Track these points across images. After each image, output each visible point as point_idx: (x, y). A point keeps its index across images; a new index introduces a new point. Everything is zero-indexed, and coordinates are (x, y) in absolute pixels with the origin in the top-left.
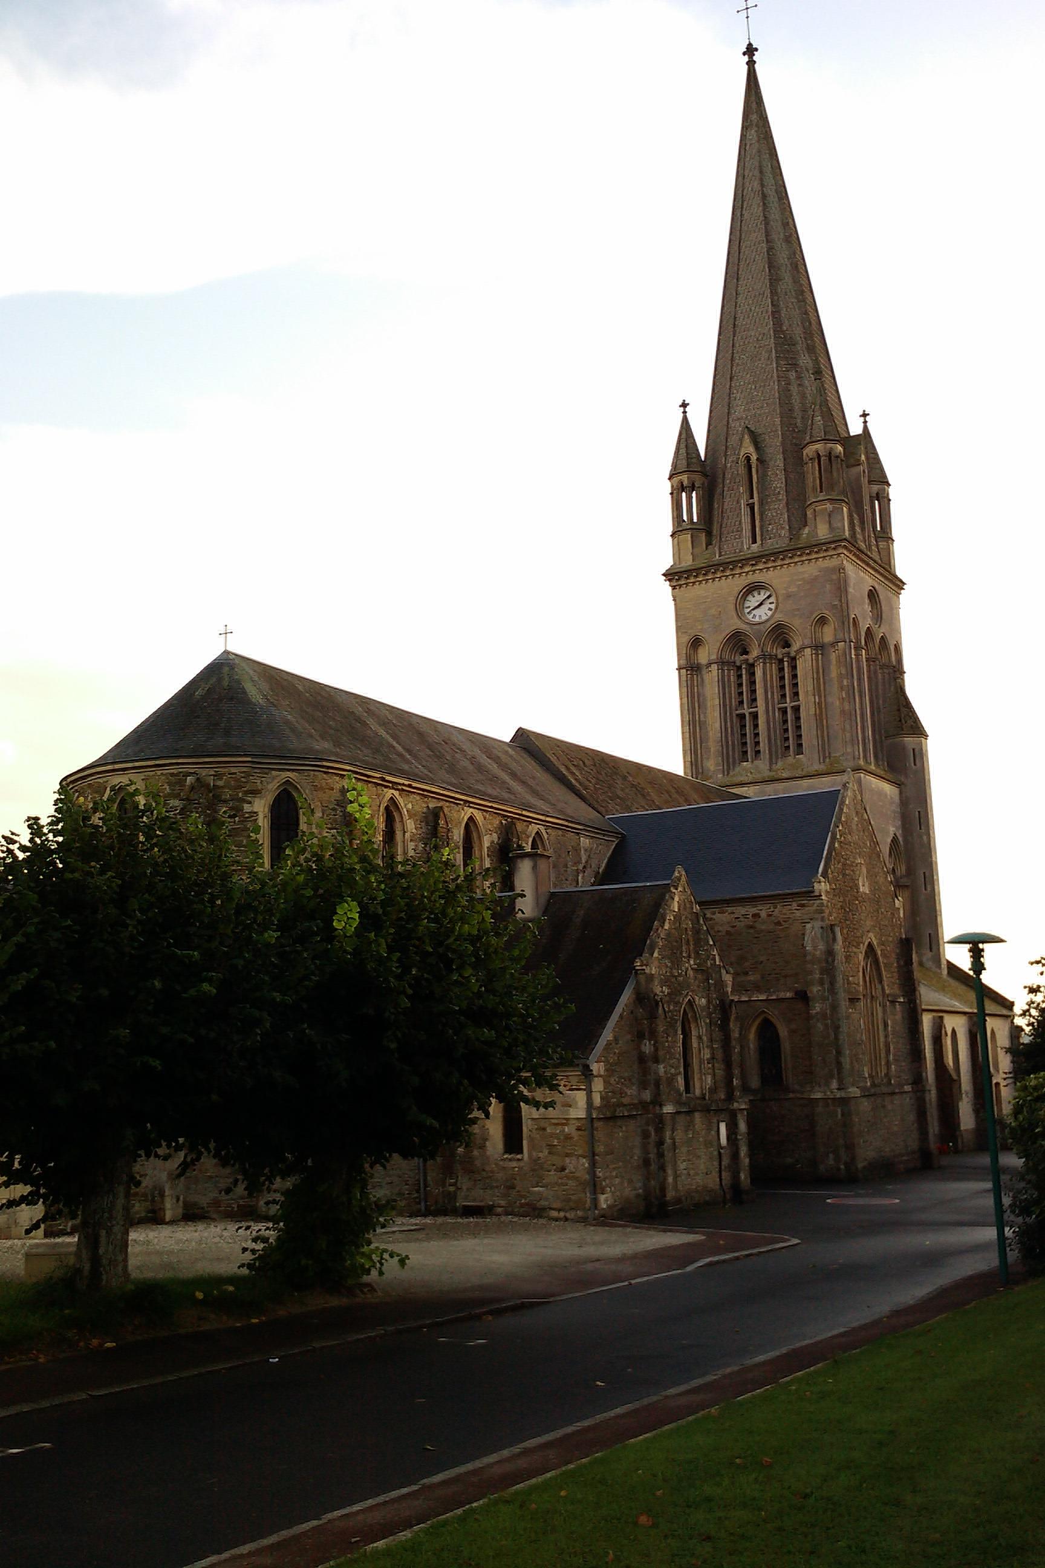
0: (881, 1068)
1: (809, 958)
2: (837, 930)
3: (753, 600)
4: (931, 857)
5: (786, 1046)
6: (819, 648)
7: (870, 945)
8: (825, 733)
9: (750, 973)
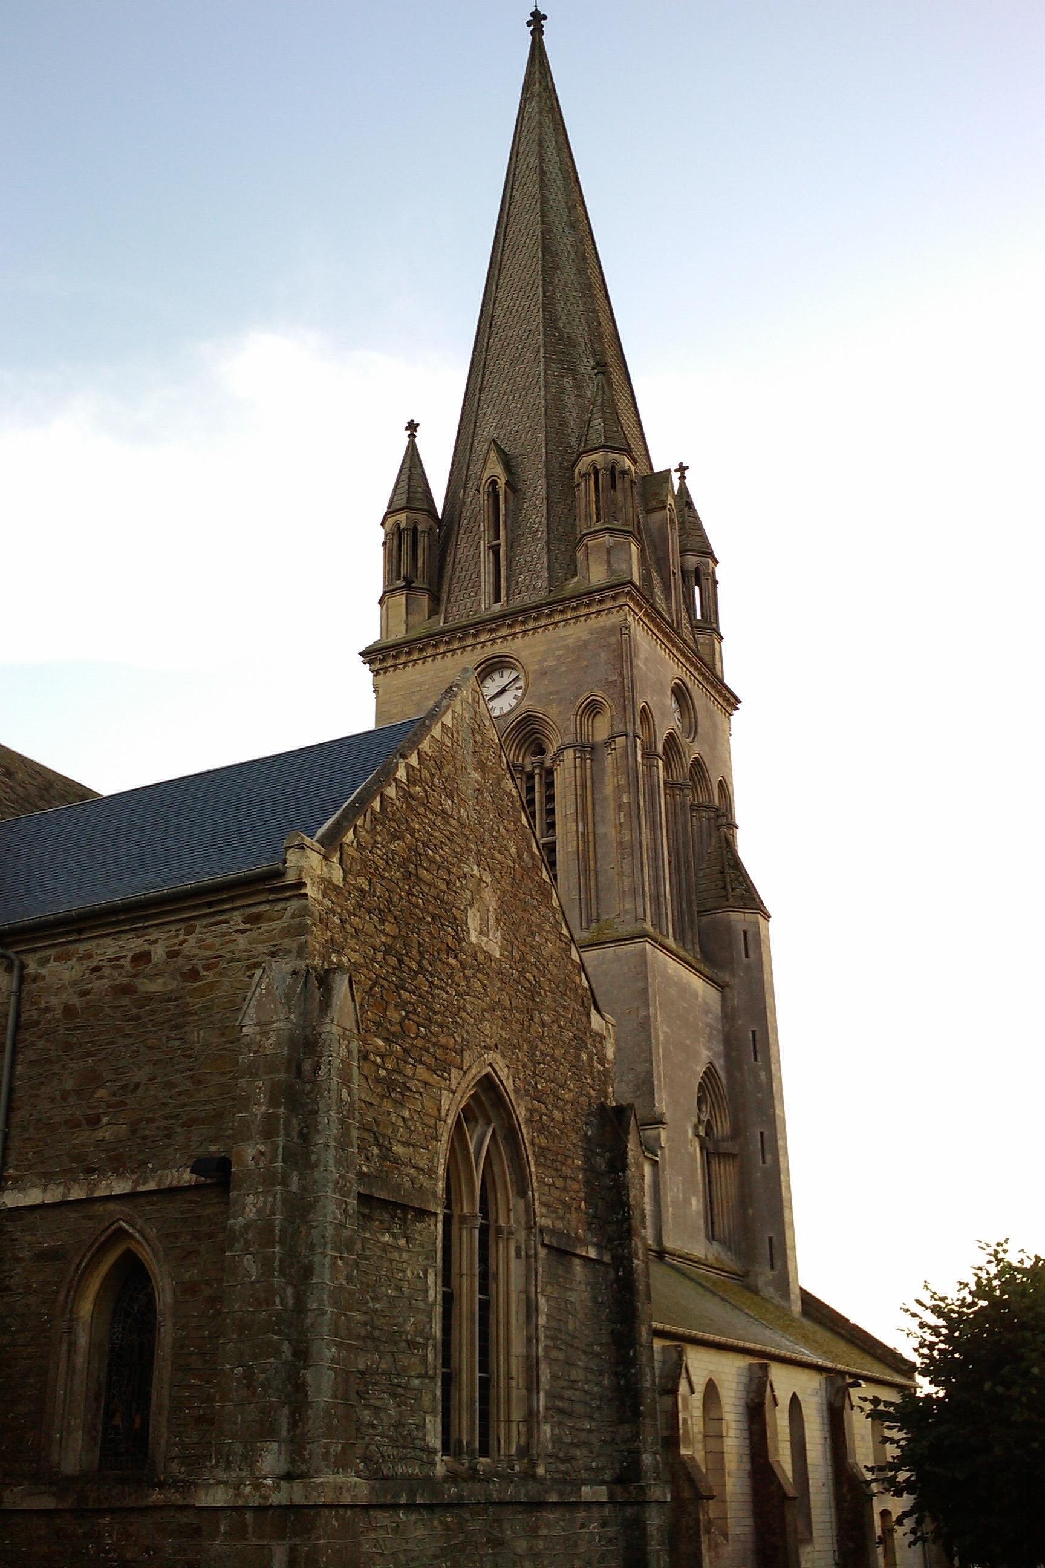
0: (509, 1431)
1: (246, 1058)
2: (341, 986)
3: (492, 686)
4: (773, 1107)
5: (166, 1334)
6: (587, 749)
7: (488, 1084)
8: (593, 882)
9: (105, 1120)
